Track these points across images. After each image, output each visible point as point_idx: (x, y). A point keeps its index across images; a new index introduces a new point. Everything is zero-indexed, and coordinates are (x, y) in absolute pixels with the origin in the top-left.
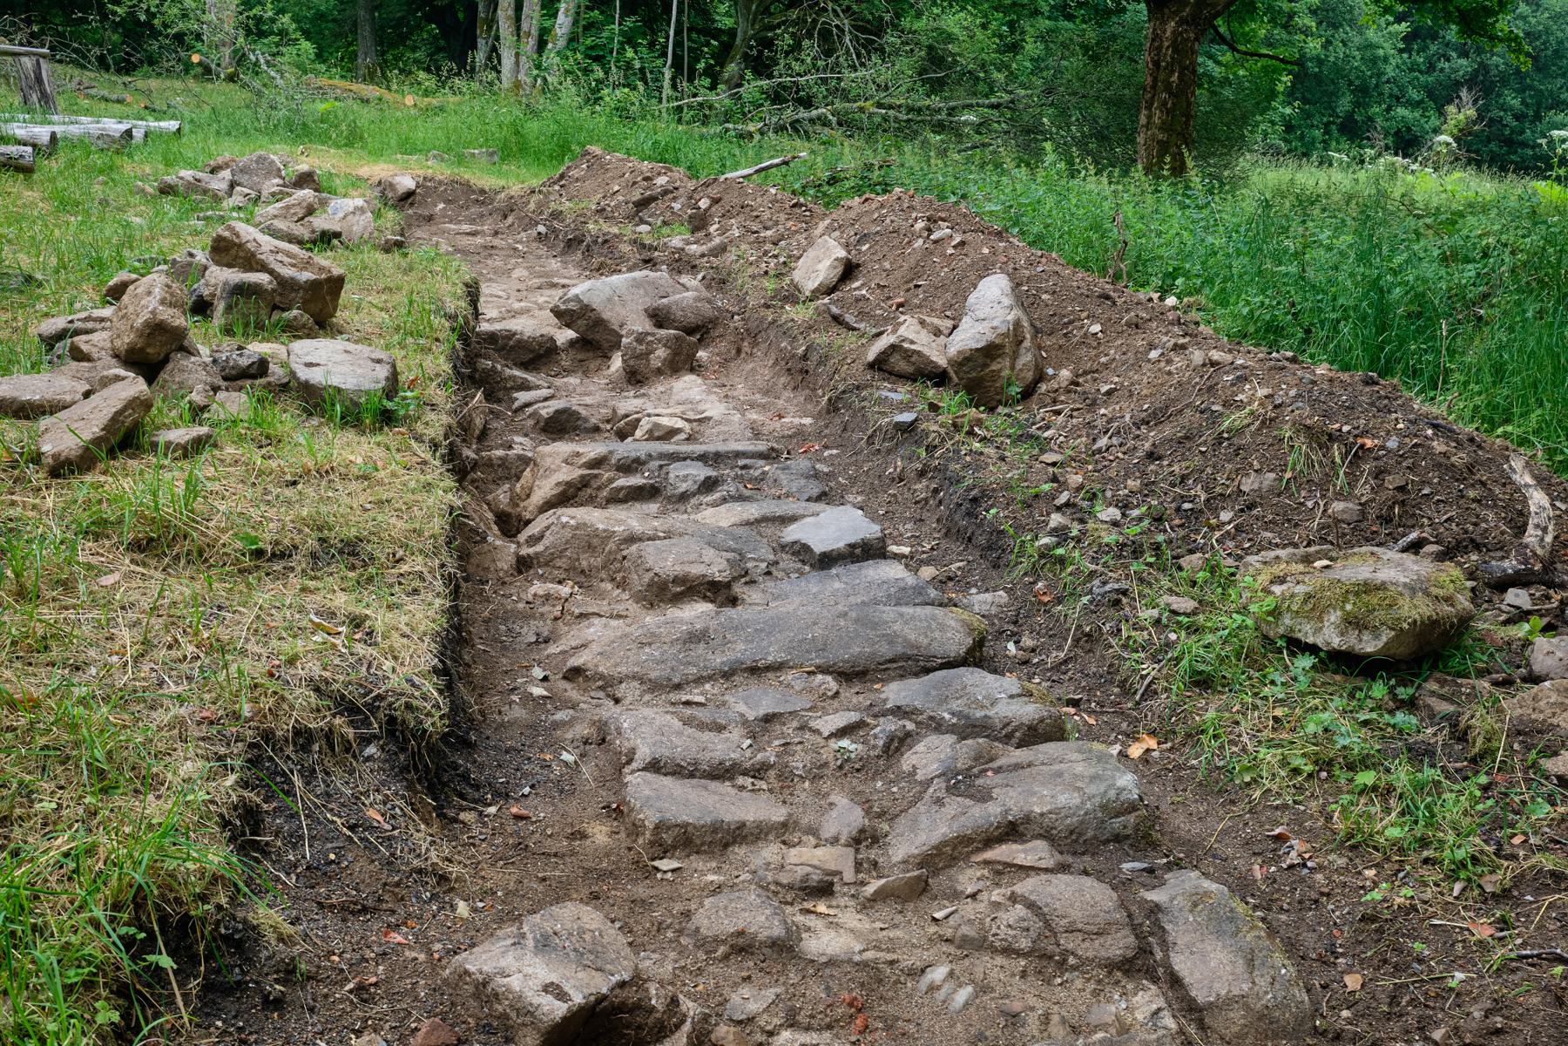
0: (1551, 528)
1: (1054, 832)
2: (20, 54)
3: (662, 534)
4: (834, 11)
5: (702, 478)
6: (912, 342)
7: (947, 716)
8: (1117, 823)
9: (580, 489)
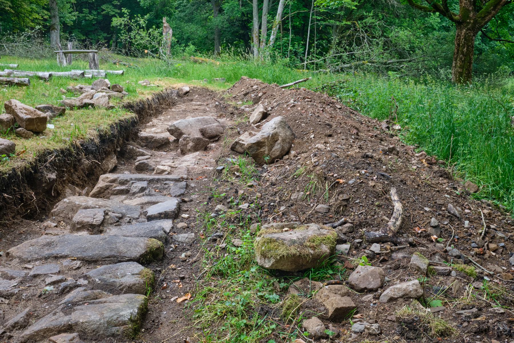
0: (400, 218)
1: (86, 330)
2: (88, 52)
3: (97, 207)
4: (362, 31)
5: (140, 187)
6: (243, 141)
7: (97, 280)
8: (114, 330)
9: (105, 190)
